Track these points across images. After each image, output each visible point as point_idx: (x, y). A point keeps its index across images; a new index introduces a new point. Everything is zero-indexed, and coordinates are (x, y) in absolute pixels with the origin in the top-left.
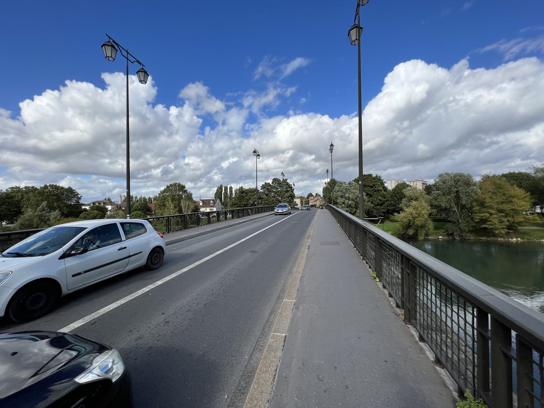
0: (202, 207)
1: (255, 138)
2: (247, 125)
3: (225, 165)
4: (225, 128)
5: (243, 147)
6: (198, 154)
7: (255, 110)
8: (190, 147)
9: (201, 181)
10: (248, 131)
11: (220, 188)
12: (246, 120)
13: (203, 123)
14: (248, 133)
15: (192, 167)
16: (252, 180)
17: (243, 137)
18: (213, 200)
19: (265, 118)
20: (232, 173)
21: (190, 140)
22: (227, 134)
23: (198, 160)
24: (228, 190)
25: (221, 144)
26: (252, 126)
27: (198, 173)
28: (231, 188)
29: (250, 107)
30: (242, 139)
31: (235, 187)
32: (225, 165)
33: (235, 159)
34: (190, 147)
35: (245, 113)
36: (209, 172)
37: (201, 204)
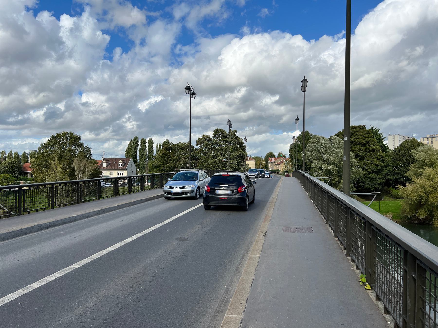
0: (106, 169)
1: (190, 67)
2: (179, 46)
3: (143, 106)
4: (145, 51)
5: (172, 80)
6: (102, 89)
7: (191, 24)
8: (91, 78)
9: (106, 130)
10: (179, 56)
11: (134, 142)
12: (176, 39)
13: (110, 42)
14: (179, 60)
15: (92, 109)
16: (183, 131)
17: (172, 64)
18: (123, 160)
19: (206, 37)
20: (156, 119)
21: (91, 67)
22: (148, 60)
23: (103, 98)
24: (147, 145)
25: (139, 75)
26: (186, 48)
27: (102, 117)
28: (151, 142)
29: (183, 19)
30: (170, 68)
31: (158, 140)
32: (143, 106)
33: (159, 99)
34: (91, 78)
35: (175, 28)
36: (119, 117)
37: (104, 165)
